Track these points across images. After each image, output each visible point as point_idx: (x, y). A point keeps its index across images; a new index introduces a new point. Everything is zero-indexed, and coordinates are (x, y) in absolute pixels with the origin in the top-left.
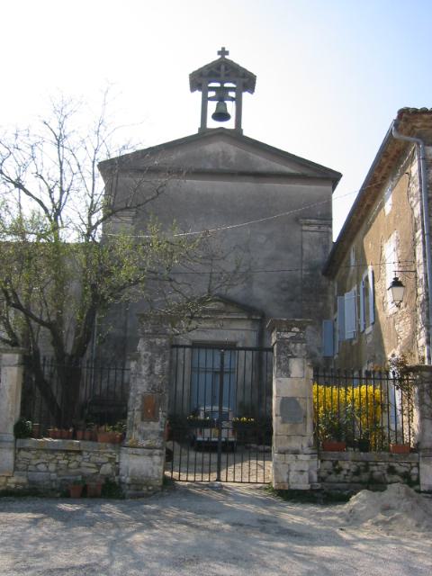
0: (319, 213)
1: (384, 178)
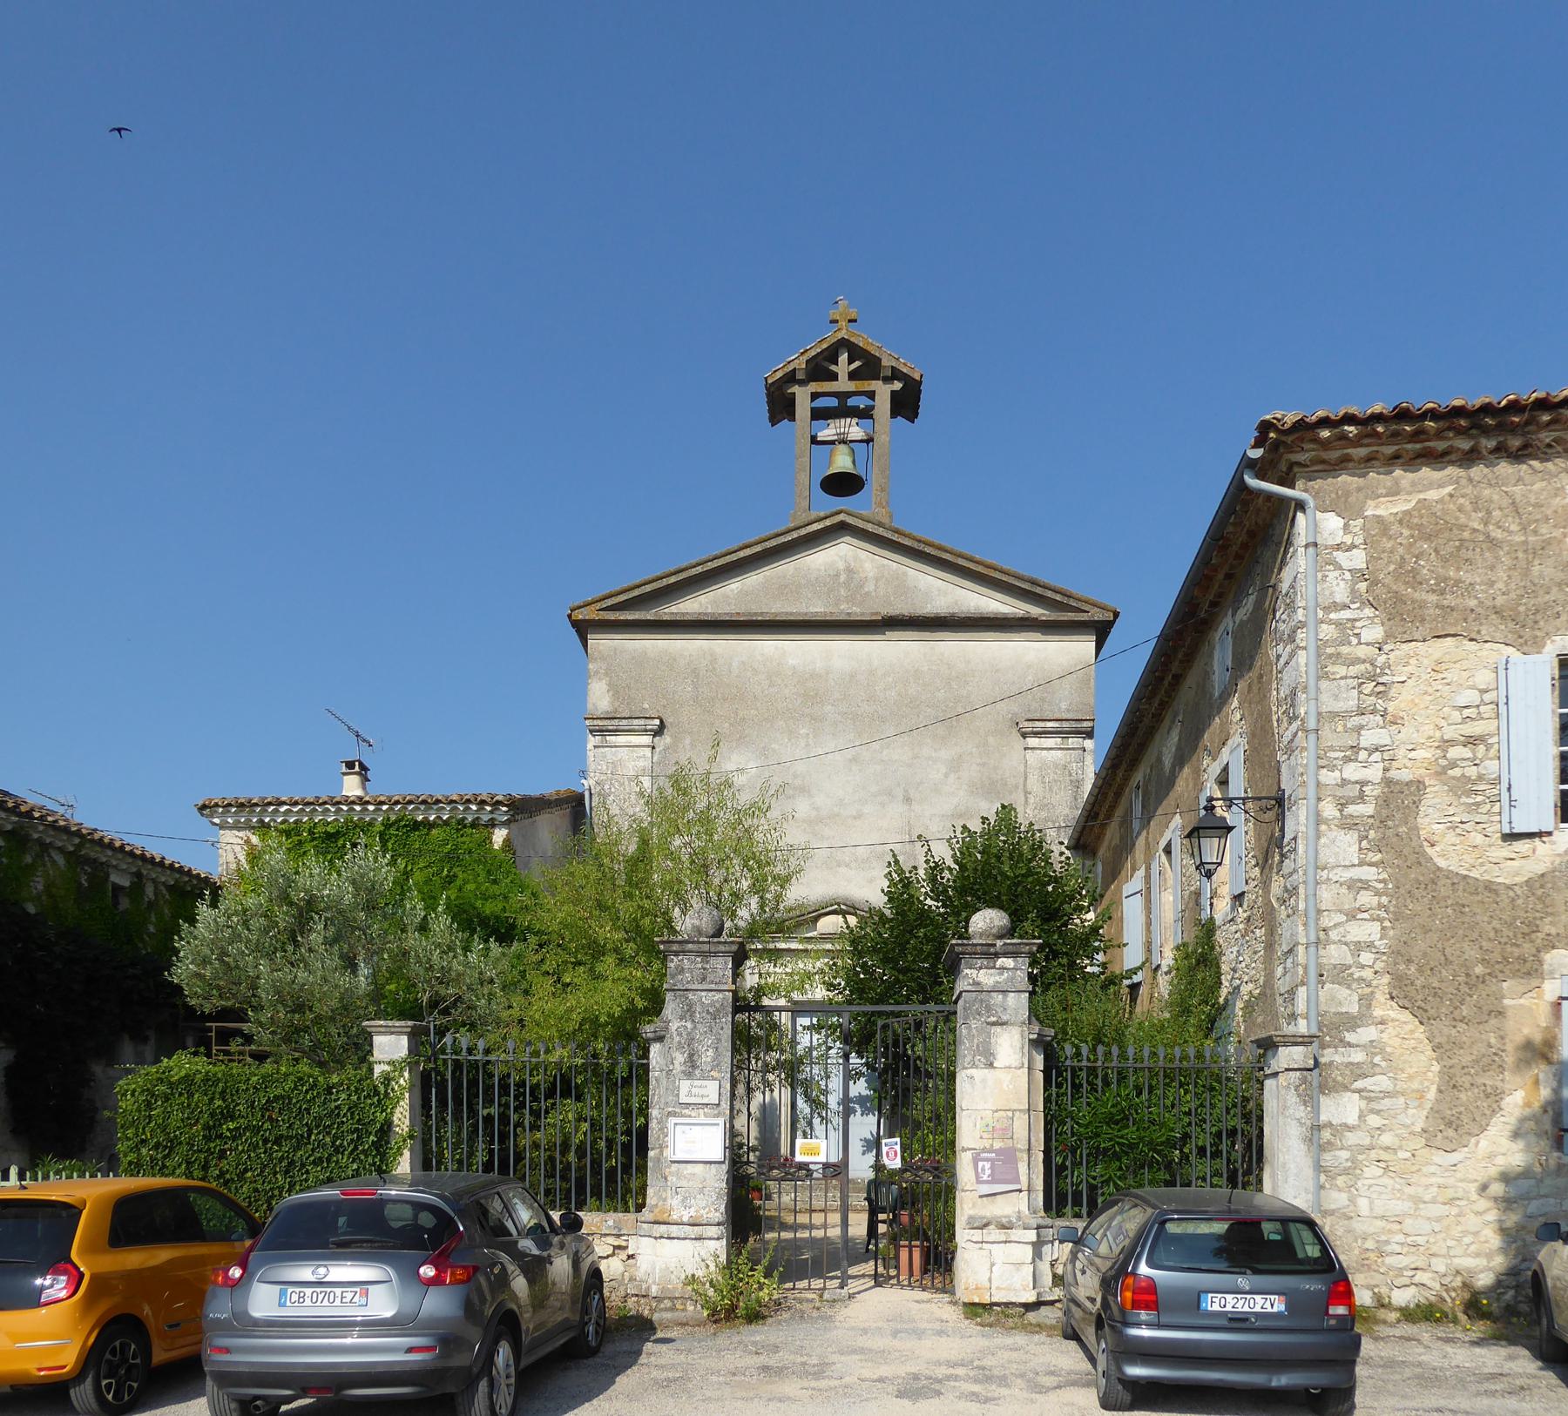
0: (1064, 706)
1: (1214, 604)
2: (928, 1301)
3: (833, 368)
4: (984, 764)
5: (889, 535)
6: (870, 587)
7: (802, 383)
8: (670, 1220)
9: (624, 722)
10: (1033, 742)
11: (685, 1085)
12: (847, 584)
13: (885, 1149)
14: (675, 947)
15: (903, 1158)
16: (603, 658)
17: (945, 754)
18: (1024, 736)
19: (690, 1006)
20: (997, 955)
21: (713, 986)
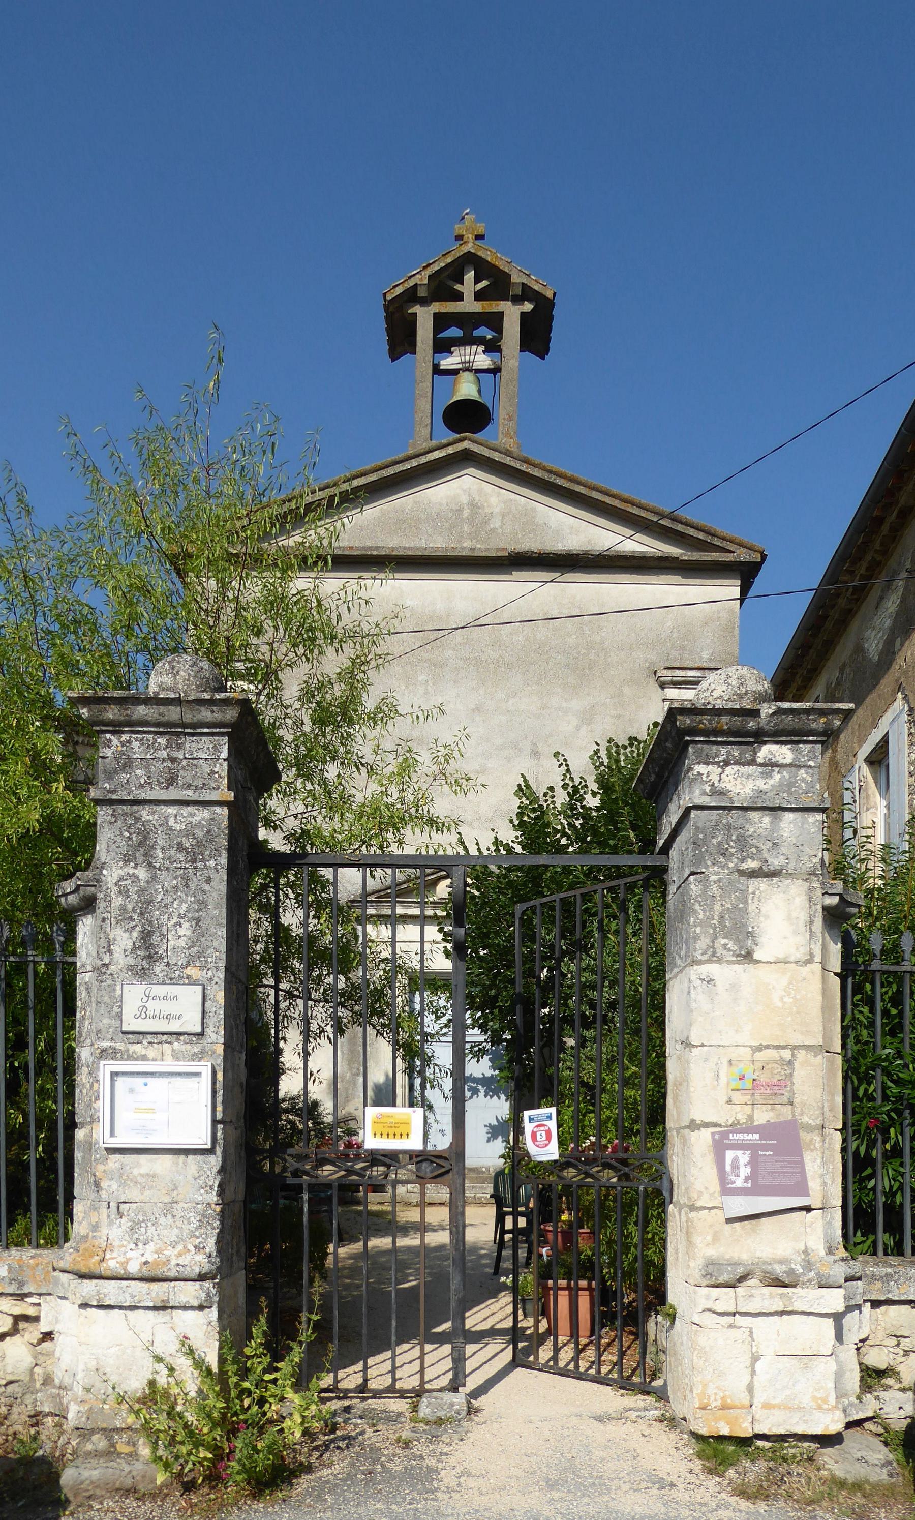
0: (705, 655)
2: (621, 1417)
3: (458, 287)
4: (619, 716)
5: (517, 465)
6: (496, 523)
7: (424, 302)
8: (103, 1269)
11: (133, 994)
12: (471, 520)
13: (528, 1127)
14: (112, 713)
15: (561, 1143)
17: (576, 704)
18: (663, 686)
19: (145, 834)
20: (759, 737)
21: (189, 794)
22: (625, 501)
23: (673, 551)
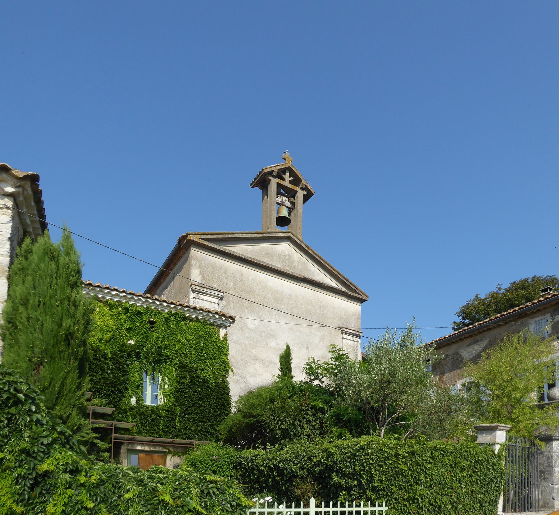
6: (296, 264)
9: (209, 290)
10: (345, 336)
16: (198, 260)
17: (319, 334)
18: (342, 333)
22: (334, 270)
23: (343, 289)
